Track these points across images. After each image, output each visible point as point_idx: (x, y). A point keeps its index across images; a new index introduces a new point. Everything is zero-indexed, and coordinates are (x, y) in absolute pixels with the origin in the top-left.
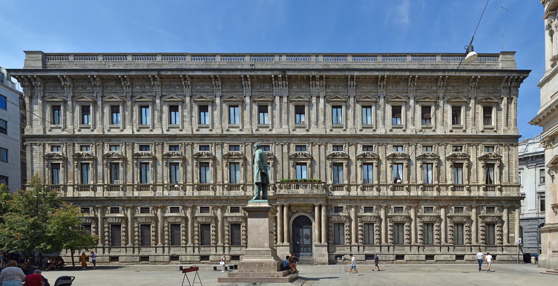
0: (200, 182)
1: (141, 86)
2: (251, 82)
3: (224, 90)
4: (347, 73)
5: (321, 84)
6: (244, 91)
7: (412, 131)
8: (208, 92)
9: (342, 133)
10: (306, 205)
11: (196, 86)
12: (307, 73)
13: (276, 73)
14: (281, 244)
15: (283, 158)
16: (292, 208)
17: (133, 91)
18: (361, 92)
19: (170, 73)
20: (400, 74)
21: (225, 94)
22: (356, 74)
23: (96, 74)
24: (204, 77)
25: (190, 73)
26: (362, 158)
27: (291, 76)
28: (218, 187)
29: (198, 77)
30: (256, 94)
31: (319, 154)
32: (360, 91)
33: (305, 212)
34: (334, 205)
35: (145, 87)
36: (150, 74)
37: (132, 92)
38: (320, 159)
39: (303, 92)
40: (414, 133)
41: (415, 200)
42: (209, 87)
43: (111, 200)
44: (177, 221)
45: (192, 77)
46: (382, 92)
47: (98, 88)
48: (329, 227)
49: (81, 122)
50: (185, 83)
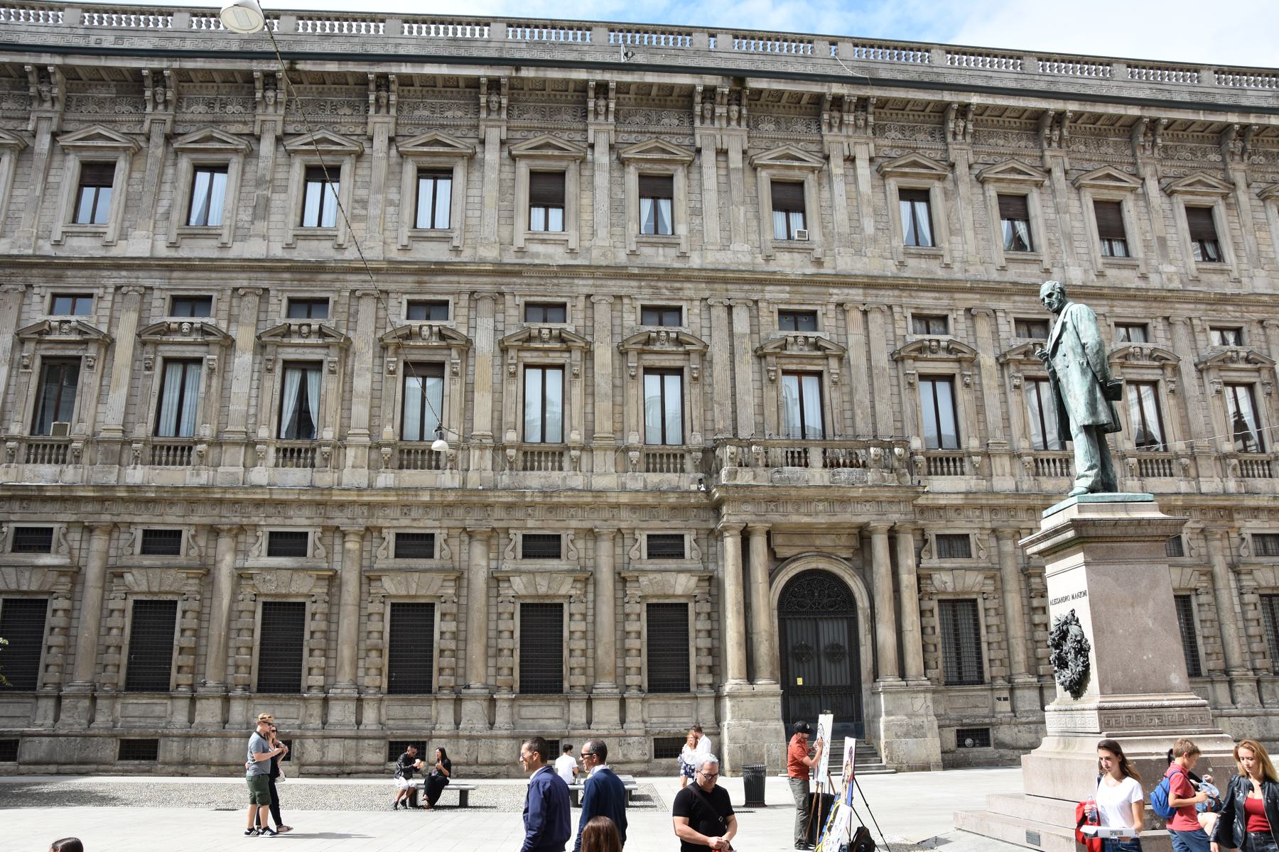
0: (401, 439)
1: (210, 104)
2: (617, 104)
3: (514, 123)
4: (947, 97)
5: (861, 123)
6: (33, 117)
7: (1170, 280)
8: (457, 127)
9: (941, 273)
10: (832, 529)
11: (415, 107)
12: (816, 88)
13: (711, 80)
14: (489, 733)
15: (732, 354)
16: (778, 540)
17: (180, 117)
18: (989, 154)
19: (332, 67)
20: (1112, 109)
21: (518, 135)
22: (975, 99)
23: (58, 60)
24: (451, 83)
25: (406, 69)
26: (1020, 362)
27: (760, 91)
28: (475, 454)
29: (430, 83)
30: (632, 138)
31: (868, 344)
32: (986, 149)
33: (828, 556)
34: (937, 527)
35: (224, 105)
36: (258, 67)
37: (174, 122)
38: (869, 360)
39: (798, 141)
40: (1176, 284)
41: (1219, 508)
42: (459, 114)
43: (22, 499)
44: (294, 589)
45: (406, 81)
46: (1056, 159)
47: (47, 105)
48: (710, 651)
49: (70, 218)
50: (377, 100)
